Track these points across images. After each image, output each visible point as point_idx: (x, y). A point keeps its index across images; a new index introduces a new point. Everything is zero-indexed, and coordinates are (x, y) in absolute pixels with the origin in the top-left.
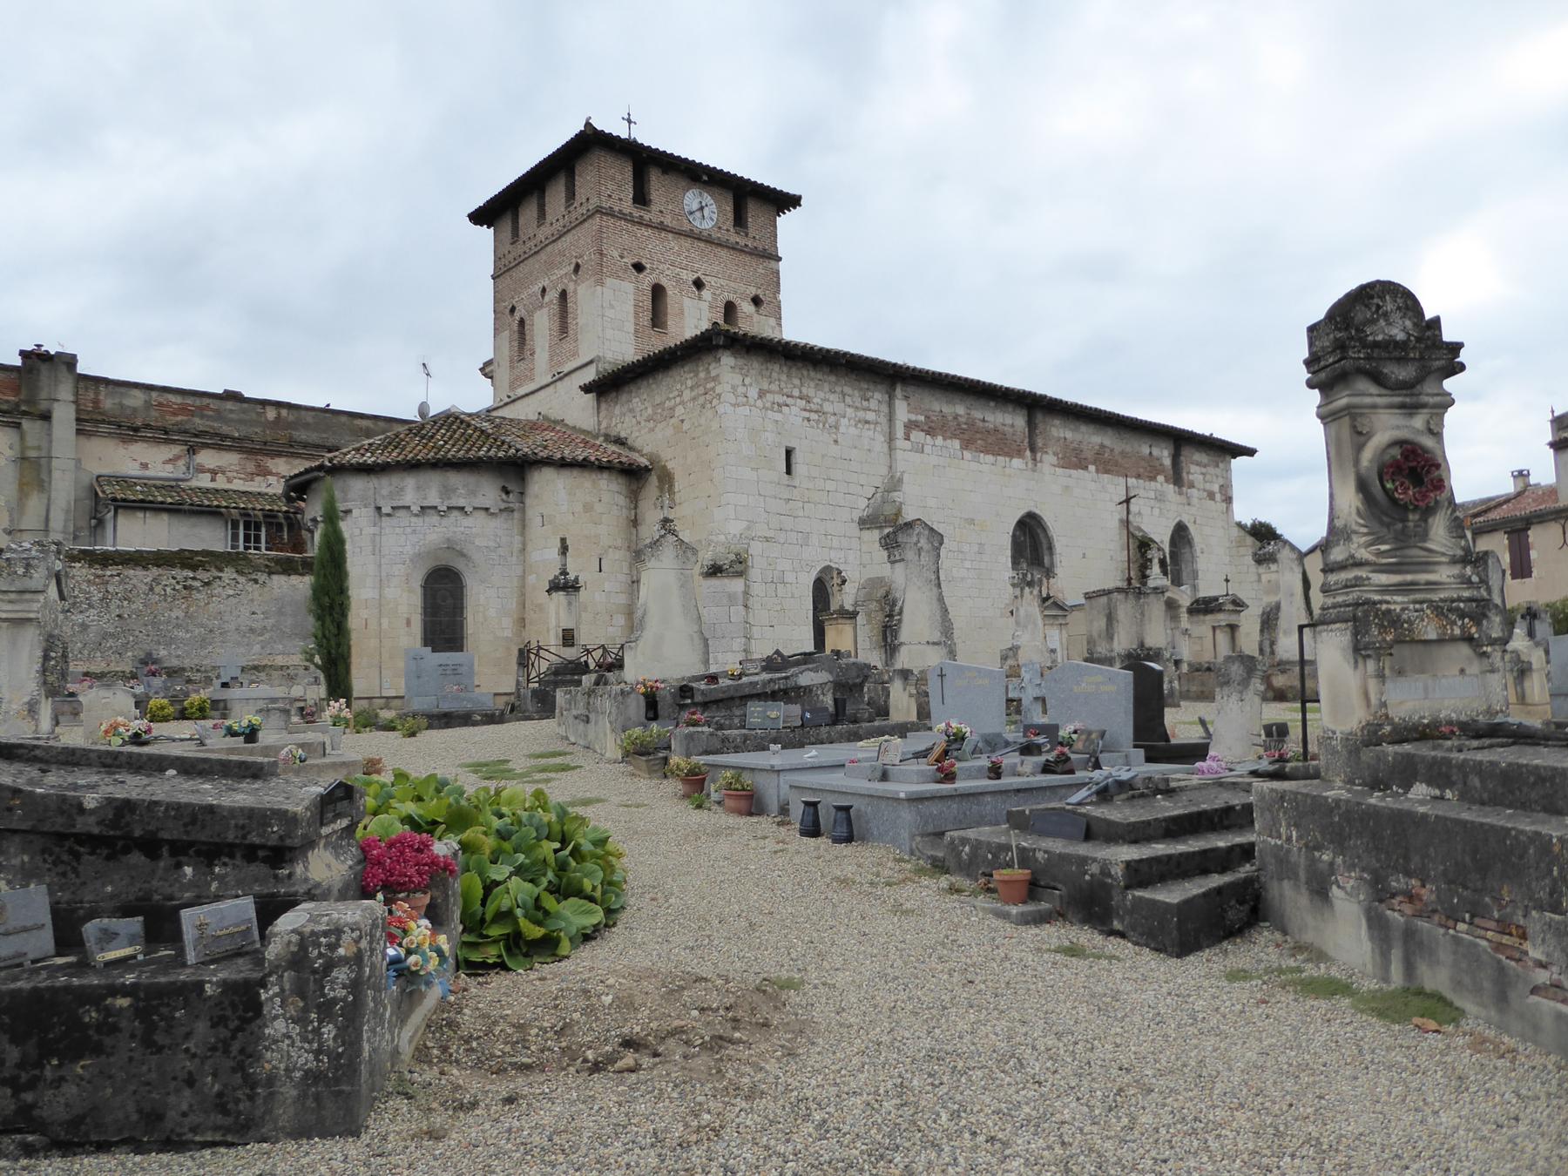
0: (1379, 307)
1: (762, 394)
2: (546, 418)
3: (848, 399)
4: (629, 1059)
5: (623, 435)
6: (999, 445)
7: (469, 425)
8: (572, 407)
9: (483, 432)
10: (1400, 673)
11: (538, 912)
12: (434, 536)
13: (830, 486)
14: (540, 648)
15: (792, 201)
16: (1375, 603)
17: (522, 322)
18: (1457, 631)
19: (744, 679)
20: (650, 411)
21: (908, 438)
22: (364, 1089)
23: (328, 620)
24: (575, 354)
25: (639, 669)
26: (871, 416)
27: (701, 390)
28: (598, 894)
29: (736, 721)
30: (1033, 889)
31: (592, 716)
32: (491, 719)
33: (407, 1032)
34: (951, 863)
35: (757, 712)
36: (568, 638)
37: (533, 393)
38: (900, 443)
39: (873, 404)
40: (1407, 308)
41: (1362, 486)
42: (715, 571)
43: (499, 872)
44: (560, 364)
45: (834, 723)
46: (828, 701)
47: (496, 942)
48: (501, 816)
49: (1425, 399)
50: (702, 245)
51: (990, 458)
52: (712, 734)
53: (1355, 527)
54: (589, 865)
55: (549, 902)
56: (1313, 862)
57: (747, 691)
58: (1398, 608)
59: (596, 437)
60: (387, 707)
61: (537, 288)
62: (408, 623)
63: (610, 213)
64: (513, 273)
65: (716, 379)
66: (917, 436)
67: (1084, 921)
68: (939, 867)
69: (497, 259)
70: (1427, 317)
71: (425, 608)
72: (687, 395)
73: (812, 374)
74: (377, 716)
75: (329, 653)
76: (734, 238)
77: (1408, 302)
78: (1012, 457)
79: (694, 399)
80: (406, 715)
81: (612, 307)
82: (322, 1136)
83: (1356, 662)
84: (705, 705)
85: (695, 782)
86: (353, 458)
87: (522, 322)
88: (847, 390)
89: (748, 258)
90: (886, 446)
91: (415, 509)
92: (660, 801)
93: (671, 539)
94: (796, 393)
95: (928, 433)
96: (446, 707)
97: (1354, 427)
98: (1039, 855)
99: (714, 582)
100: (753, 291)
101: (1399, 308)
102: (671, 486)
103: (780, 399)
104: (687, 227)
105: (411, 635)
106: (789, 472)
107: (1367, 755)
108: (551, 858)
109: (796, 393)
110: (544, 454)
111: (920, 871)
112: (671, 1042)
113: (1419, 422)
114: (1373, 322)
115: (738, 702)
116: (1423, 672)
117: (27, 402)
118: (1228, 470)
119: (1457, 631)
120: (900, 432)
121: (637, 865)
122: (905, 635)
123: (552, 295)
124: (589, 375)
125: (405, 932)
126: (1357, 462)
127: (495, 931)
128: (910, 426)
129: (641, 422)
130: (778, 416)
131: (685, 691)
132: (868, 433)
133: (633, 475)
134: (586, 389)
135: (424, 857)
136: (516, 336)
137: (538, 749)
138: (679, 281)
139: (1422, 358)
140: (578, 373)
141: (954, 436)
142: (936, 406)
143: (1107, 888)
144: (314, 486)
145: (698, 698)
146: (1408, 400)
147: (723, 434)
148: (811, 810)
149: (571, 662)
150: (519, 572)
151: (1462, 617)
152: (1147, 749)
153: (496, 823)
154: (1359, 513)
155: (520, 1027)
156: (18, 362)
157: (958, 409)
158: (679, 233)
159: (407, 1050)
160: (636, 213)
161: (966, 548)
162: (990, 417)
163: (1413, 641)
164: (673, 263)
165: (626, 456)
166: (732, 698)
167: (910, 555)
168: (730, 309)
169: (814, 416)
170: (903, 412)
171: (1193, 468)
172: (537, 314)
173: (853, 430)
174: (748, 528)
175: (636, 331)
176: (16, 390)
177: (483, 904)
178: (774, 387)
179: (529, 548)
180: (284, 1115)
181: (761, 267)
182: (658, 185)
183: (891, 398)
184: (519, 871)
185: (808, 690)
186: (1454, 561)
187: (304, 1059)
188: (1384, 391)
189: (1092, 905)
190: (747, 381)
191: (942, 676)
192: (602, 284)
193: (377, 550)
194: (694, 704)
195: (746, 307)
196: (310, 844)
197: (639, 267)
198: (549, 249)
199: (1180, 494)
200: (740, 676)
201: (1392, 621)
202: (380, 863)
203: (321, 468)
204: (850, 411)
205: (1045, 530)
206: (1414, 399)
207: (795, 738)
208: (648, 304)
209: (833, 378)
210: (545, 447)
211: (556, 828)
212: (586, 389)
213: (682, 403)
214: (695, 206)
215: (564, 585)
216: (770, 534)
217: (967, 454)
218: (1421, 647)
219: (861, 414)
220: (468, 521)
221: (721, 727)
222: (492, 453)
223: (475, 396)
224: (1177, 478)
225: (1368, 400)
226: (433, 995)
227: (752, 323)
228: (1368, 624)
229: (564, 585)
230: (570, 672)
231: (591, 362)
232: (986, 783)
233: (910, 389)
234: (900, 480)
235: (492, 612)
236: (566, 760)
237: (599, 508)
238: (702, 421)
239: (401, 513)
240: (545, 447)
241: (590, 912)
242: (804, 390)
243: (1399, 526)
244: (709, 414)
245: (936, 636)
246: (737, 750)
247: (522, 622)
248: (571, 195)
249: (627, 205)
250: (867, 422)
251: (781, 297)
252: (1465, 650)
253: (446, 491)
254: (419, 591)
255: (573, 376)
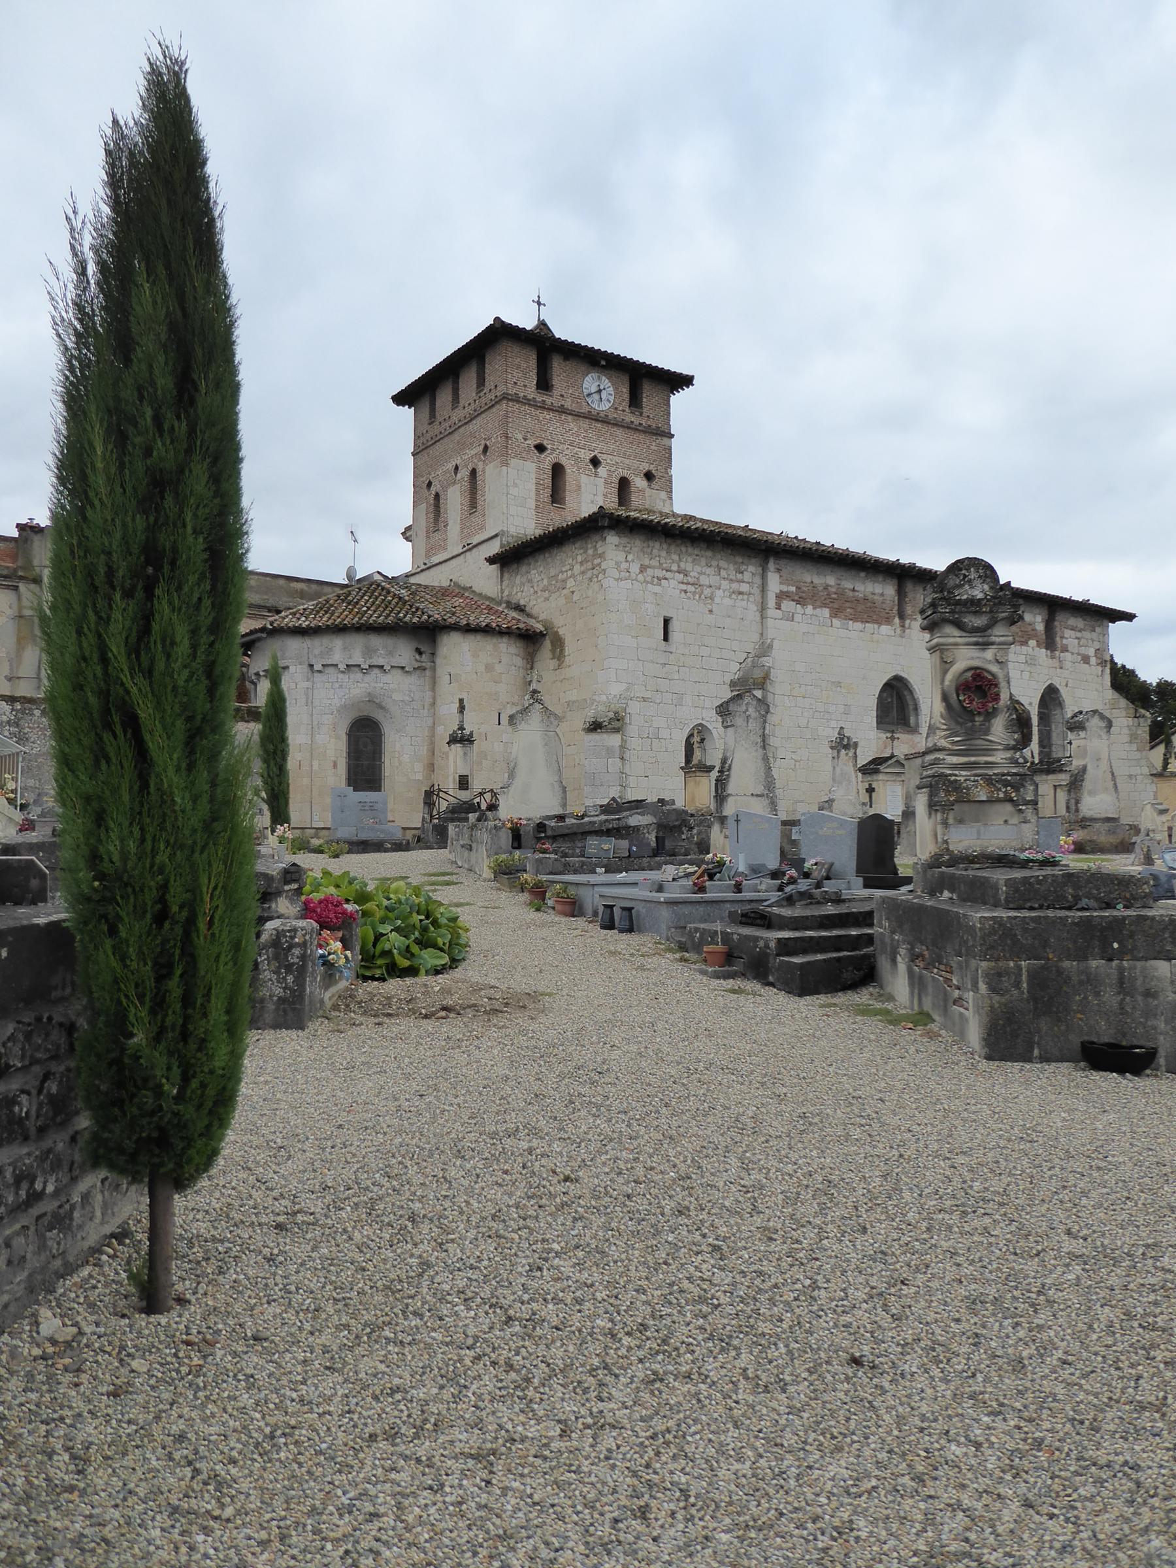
0: (965, 576)
1: (643, 569)
2: (457, 585)
3: (723, 573)
4: (443, 1013)
5: (522, 603)
6: (867, 613)
7: (389, 592)
8: (480, 576)
9: (400, 598)
10: (961, 821)
11: (407, 952)
12: (358, 691)
13: (705, 651)
14: (440, 790)
15: (681, 381)
16: (946, 776)
17: (437, 496)
18: (1001, 795)
19: (586, 819)
20: (545, 582)
21: (779, 608)
22: (307, 1008)
23: (272, 763)
24: (482, 528)
25: (509, 810)
26: (744, 587)
27: (589, 565)
28: (446, 948)
29: (578, 851)
30: (729, 957)
31: (474, 845)
32: (399, 847)
33: (328, 995)
34: (689, 945)
35: (594, 845)
36: (464, 783)
37: (440, 563)
38: (772, 612)
39: (747, 576)
40: (986, 576)
41: (945, 698)
42: (595, 727)
43: (385, 929)
44: (469, 536)
45: (655, 855)
46: (652, 838)
47: (380, 967)
48: (389, 899)
49: (993, 639)
50: (599, 425)
51: (859, 626)
52: (556, 860)
53: (939, 725)
54: (443, 931)
55: (415, 949)
56: (893, 939)
57: (587, 829)
58: (962, 779)
59: (499, 603)
60: (317, 836)
61: (450, 466)
62: (335, 766)
63: (516, 399)
64: (430, 451)
65: (601, 556)
66: (788, 605)
67: (754, 978)
68: (682, 947)
69: (417, 437)
70: (1002, 582)
71: (349, 754)
72: (577, 569)
73: (690, 550)
74: (308, 842)
75: (273, 789)
76: (629, 418)
77: (988, 572)
78: (880, 624)
79: (583, 573)
80: (332, 841)
81: (515, 485)
82: (287, 1029)
83: (930, 814)
84: (554, 838)
85: (538, 893)
86: (288, 621)
87: (437, 496)
88: (723, 564)
89: (642, 436)
90: (758, 614)
91: (342, 667)
92: (513, 906)
93: (538, 706)
94: (674, 567)
95: (798, 603)
96: (363, 836)
97: (942, 658)
98: (735, 937)
99: (595, 737)
100: (645, 467)
101: (980, 577)
102: (562, 650)
103: (659, 573)
104: (585, 409)
105: (337, 776)
106: (666, 639)
107: (930, 872)
108: (418, 925)
109: (674, 567)
110: (452, 620)
111: (670, 950)
112: (468, 1010)
113: (989, 654)
114: (960, 586)
115: (580, 837)
116: (977, 822)
117: (23, 568)
118: (1105, 634)
119: (1001, 795)
120: (771, 602)
121: (476, 937)
122: (731, 788)
123: (464, 473)
124: (494, 548)
125: (328, 944)
126: (943, 681)
127: (380, 962)
128: (781, 596)
129: (540, 592)
130: (657, 589)
131: (541, 827)
132: (741, 603)
133: (531, 639)
134: (491, 560)
135: (339, 909)
136: (432, 508)
137: (431, 870)
138: (577, 458)
139: (991, 612)
140: (484, 546)
141: (825, 605)
142: (808, 578)
143: (767, 955)
144: (257, 644)
145: (549, 833)
146: (980, 640)
147: (612, 600)
148: (609, 911)
149: (465, 803)
150: (430, 723)
151: (1006, 786)
152: (865, 879)
153: (385, 902)
154: (942, 716)
155: (388, 998)
156: (15, 533)
157: (829, 579)
158: (578, 415)
159: (328, 1004)
160: (539, 398)
161: (832, 709)
162: (860, 587)
163: (969, 801)
164: (571, 443)
165: (523, 622)
166: (575, 834)
167: (739, 721)
168: (624, 485)
169: (691, 588)
170: (775, 583)
171: (1068, 633)
172: (451, 490)
173: (727, 601)
174: (627, 689)
175: (537, 507)
176: (14, 557)
177: (374, 945)
178: (654, 563)
179: (438, 702)
180: (268, 1017)
181: (654, 444)
182: (559, 369)
183: (764, 570)
184: (397, 930)
185: (636, 829)
186: (1008, 748)
187: (278, 991)
188: (964, 634)
189: (758, 968)
190: (630, 557)
191: (737, 821)
192: (507, 465)
193: (309, 702)
194: (547, 837)
195: (639, 482)
196: (279, 893)
197: (540, 448)
198: (462, 430)
199: (1052, 658)
200: (583, 817)
201: (955, 787)
202: (315, 911)
203: (263, 629)
204: (725, 583)
205: (911, 692)
206: (985, 639)
207: (626, 863)
208: (548, 481)
209: (709, 553)
210: (454, 614)
211: (423, 908)
212: (491, 560)
213: (573, 576)
214: (594, 389)
215: (461, 739)
216: (648, 695)
217: (836, 622)
218: (977, 805)
219: (735, 586)
220: (387, 678)
221: (565, 855)
222: (407, 619)
223: (394, 558)
224: (1049, 642)
225: (951, 640)
226: (343, 984)
227: (645, 502)
228: (938, 789)
229: (461, 739)
230: (461, 811)
231: (496, 536)
232: (731, 895)
233: (783, 562)
234: (770, 646)
235: (406, 758)
236: (453, 878)
237: (499, 668)
238: (590, 593)
239: (331, 670)
240: (454, 614)
241: (440, 957)
242: (682, 565)
243: (970, 724)
244: (596, 586)
245: (760, 789)
246: (575, 872)
247: (431, 767)
248: (481, 382)
249: (531, 391)
250: (741, 593)
251: (675, 471)
252: (1008, 807)
253: (369, 652)
254: (344, 738)
255: (480, 547)
